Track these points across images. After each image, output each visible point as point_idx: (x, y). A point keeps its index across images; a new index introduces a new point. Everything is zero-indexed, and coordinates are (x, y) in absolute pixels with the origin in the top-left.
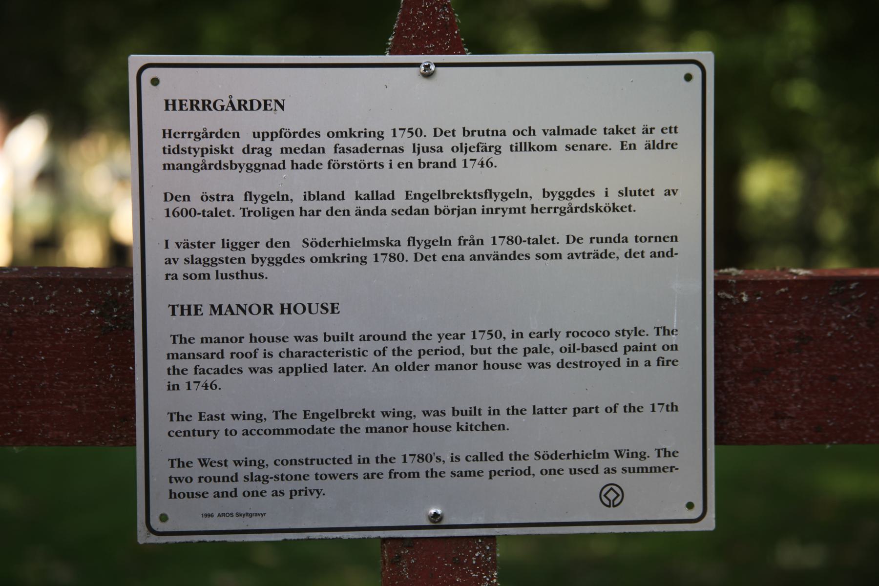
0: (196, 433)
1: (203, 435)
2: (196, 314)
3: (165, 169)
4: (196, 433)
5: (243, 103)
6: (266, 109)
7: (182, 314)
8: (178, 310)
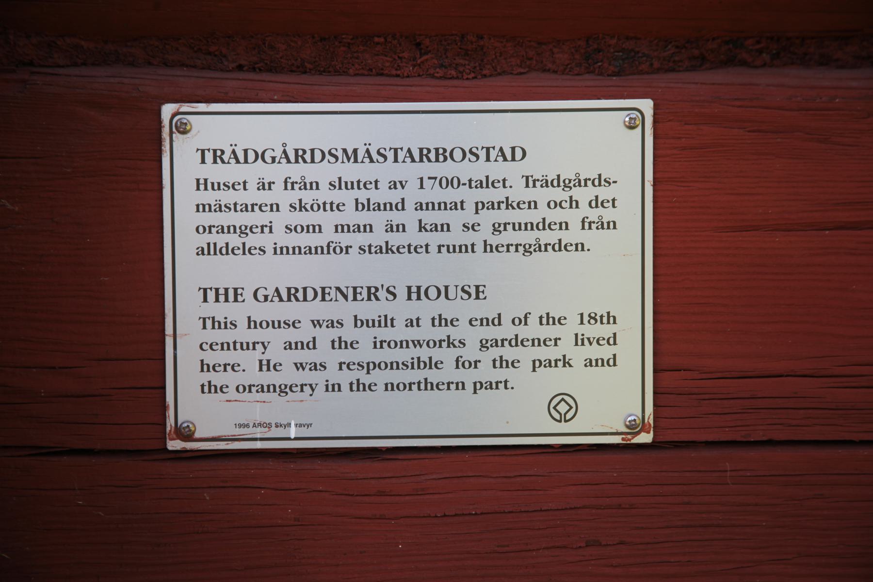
0: (238, 346)
1: (248, 348)
2: (236, 300)
3: (198, 211)
4: (238, 346)
5: (300, 153)
6: (323, 299)
7: (217, 300)
8: (211, 295)
